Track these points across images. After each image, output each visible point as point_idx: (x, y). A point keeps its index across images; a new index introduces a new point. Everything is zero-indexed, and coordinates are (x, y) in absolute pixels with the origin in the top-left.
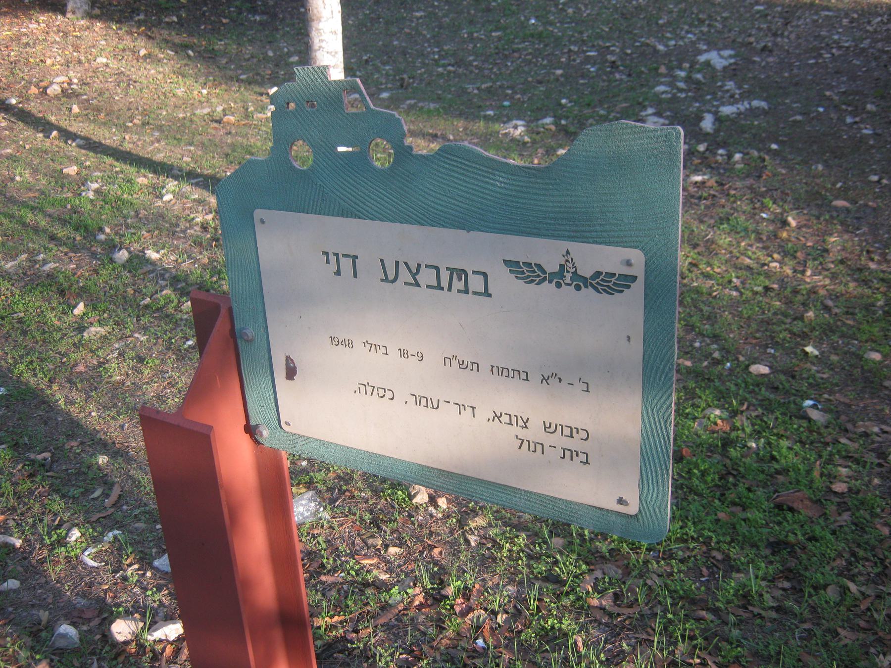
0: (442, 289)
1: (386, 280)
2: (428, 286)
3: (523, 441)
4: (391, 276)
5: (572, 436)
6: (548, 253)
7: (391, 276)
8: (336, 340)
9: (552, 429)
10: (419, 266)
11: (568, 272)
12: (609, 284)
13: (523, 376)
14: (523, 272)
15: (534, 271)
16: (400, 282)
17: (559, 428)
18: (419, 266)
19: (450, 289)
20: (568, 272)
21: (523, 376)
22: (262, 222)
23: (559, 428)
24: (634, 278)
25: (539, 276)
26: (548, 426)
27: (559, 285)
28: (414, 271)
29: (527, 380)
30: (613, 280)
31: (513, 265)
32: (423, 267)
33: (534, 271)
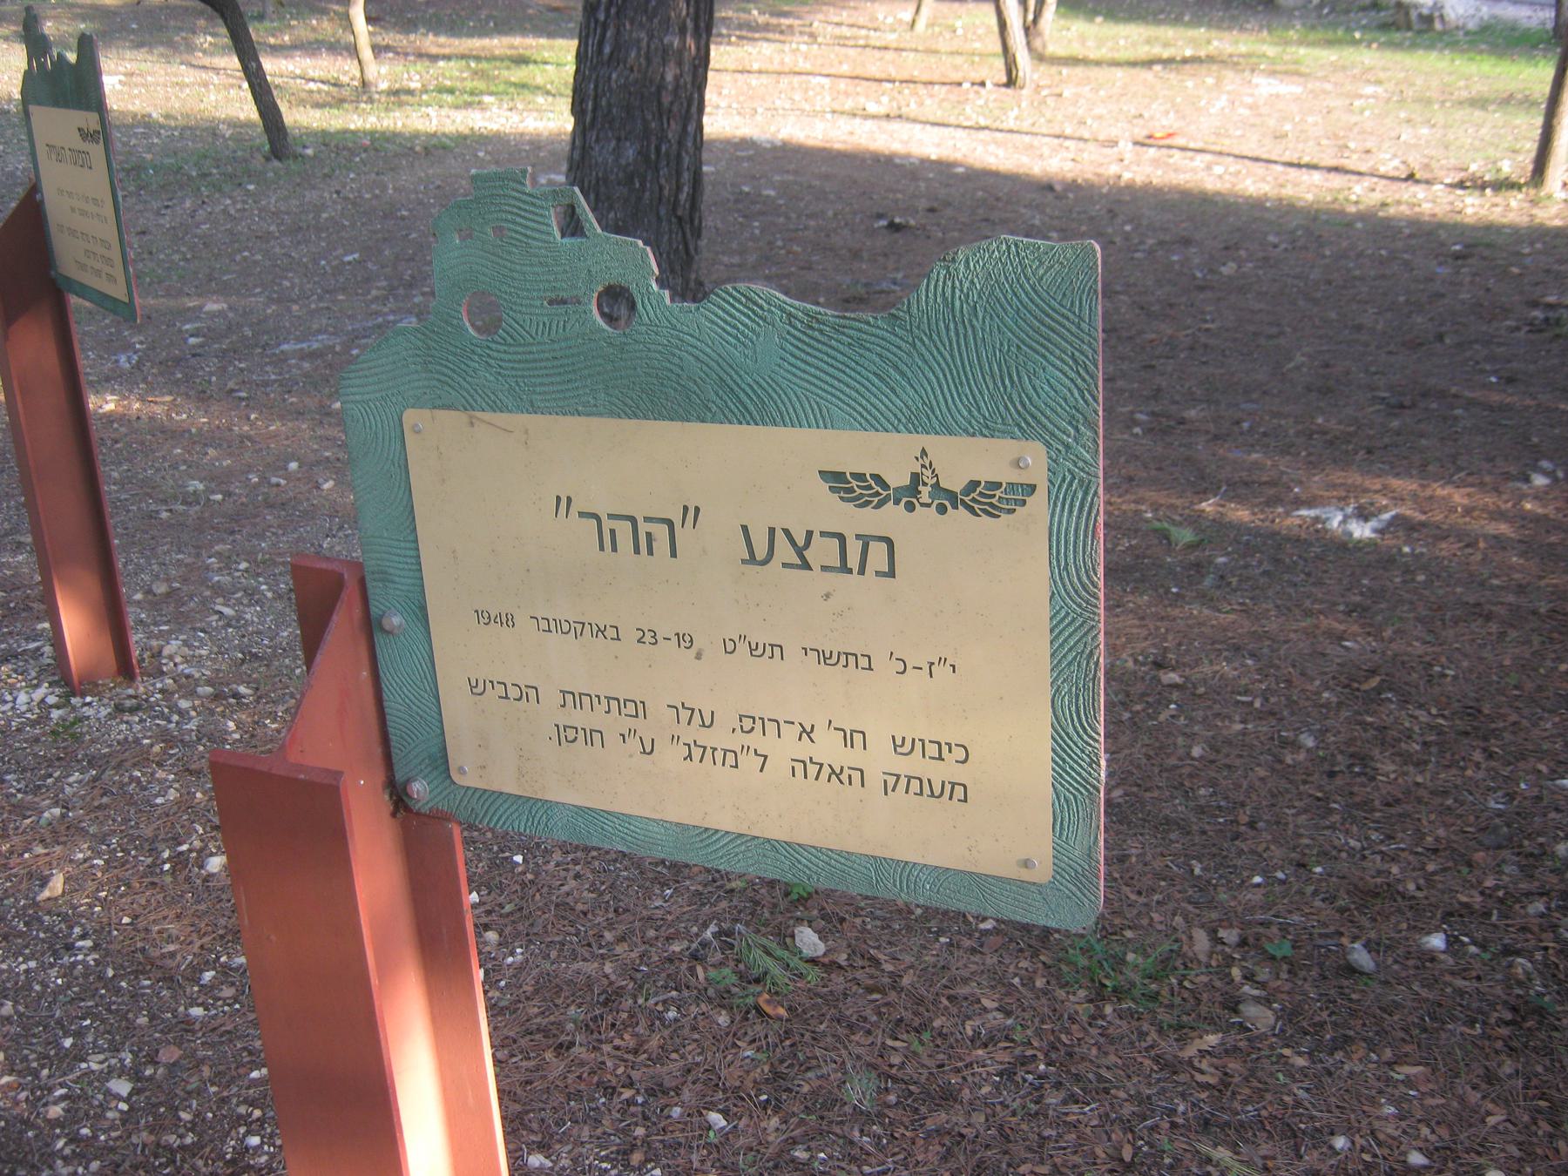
0: (850, 571)
1: (932, 795)
2: (824, 568)
3: (821, 765)
4: (761, 553)
5: (941, 758)
6: (891, 455)
7: (761, 553)
8: (687, 638)
9: (760, 651)
10: (810, 534)
11: (925, 484)
12: (983, 499)
13: (863, 662)
14: (851, 490)
15: (870, 487)
16: (776, 562)
17: (918, 745)
18: (810, 534)
19: (862, 571)
20: (925, 484)
21: (863, 662)
22: (417, 431)
23: (918, 745)
24: (1032, 488)
25: (878, 494)
26: (899, 742)
27: (910, 507)
28: (801, 543)
29: (870, 668)
30: (998, 493)
31: (835, 479)
32: (816, 535)
33: (870, 487)
